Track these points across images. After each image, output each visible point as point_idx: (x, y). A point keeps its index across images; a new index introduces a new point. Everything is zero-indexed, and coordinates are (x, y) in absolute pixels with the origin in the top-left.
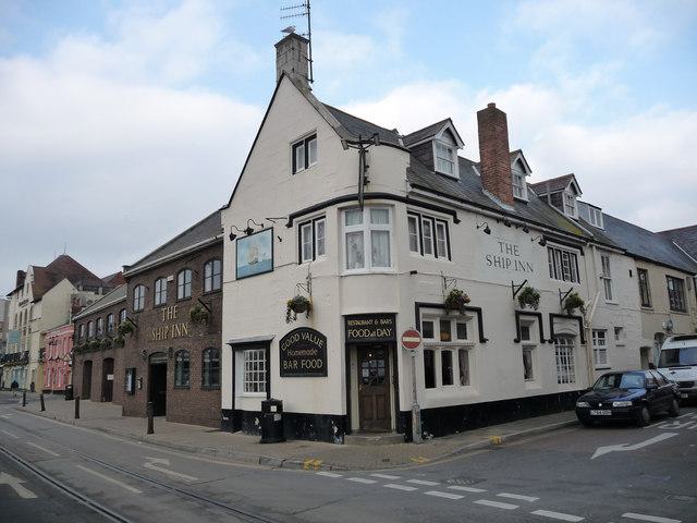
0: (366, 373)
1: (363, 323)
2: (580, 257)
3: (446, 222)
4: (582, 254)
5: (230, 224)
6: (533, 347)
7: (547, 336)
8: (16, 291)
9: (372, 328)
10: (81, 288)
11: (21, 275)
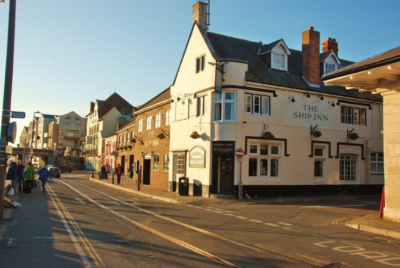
0: (224, 168)
1: (221, 145)
2: (368, 111)
3: (269, 97)
4: (370, 109)
5: (174, 92)
6: (324, 159)
7: (334, 153)
8: (90, 114)
9: (224, 147)
10: (123, 113)
11: (93, 105)
